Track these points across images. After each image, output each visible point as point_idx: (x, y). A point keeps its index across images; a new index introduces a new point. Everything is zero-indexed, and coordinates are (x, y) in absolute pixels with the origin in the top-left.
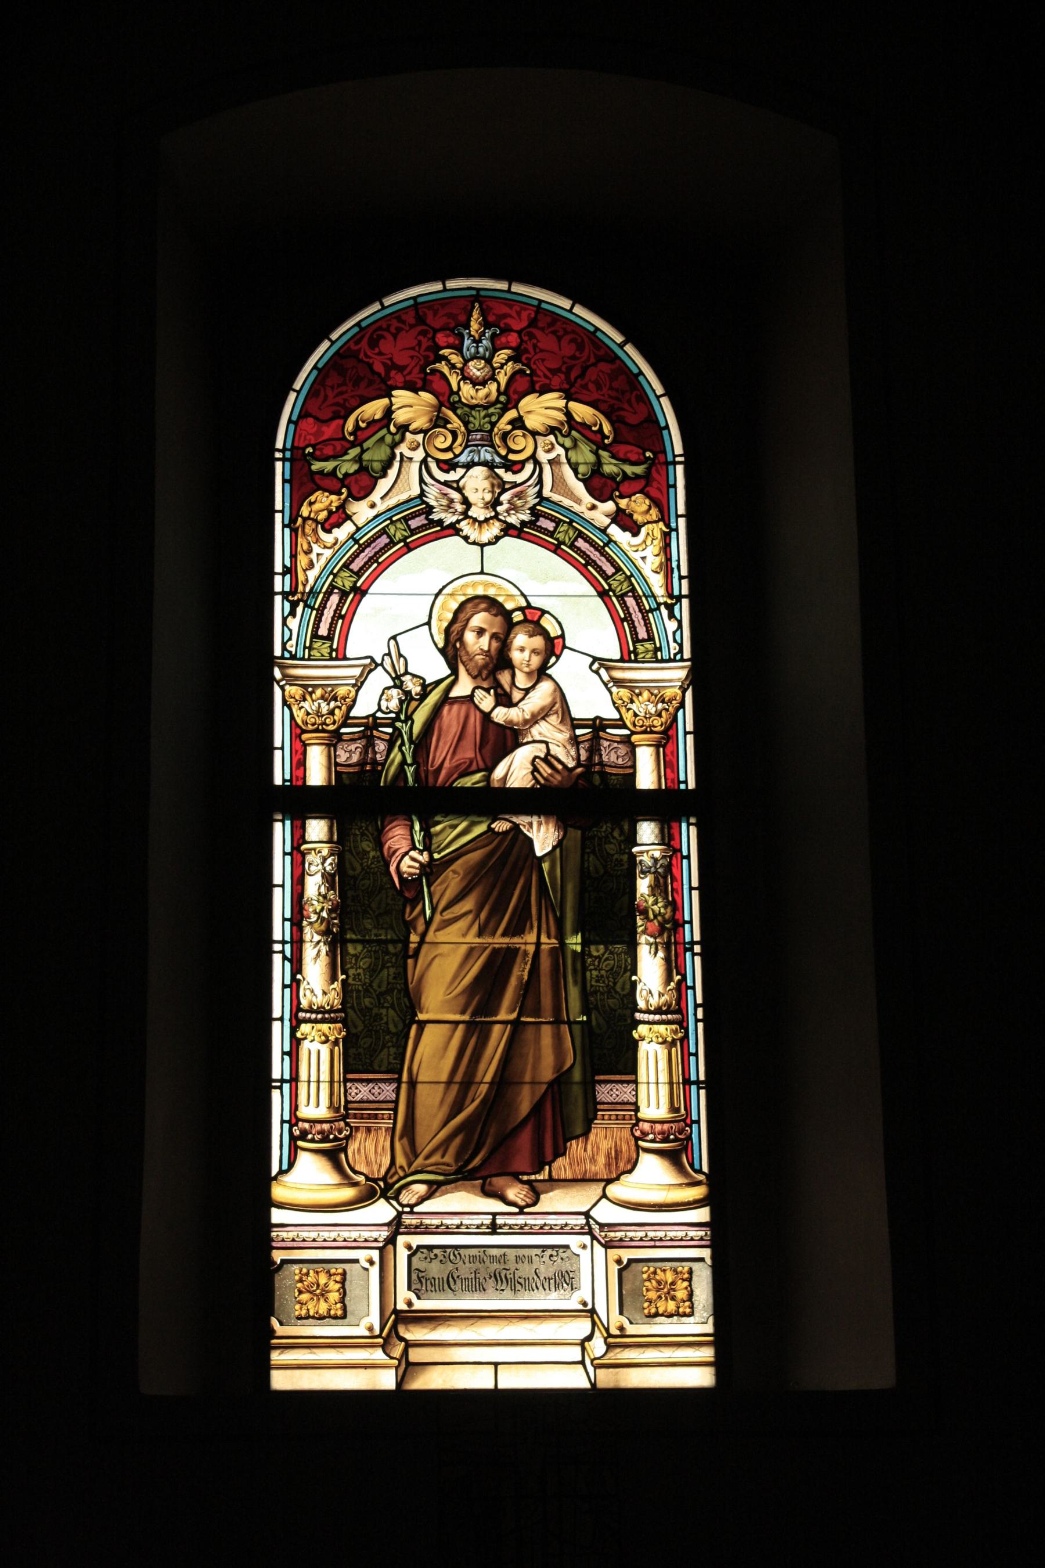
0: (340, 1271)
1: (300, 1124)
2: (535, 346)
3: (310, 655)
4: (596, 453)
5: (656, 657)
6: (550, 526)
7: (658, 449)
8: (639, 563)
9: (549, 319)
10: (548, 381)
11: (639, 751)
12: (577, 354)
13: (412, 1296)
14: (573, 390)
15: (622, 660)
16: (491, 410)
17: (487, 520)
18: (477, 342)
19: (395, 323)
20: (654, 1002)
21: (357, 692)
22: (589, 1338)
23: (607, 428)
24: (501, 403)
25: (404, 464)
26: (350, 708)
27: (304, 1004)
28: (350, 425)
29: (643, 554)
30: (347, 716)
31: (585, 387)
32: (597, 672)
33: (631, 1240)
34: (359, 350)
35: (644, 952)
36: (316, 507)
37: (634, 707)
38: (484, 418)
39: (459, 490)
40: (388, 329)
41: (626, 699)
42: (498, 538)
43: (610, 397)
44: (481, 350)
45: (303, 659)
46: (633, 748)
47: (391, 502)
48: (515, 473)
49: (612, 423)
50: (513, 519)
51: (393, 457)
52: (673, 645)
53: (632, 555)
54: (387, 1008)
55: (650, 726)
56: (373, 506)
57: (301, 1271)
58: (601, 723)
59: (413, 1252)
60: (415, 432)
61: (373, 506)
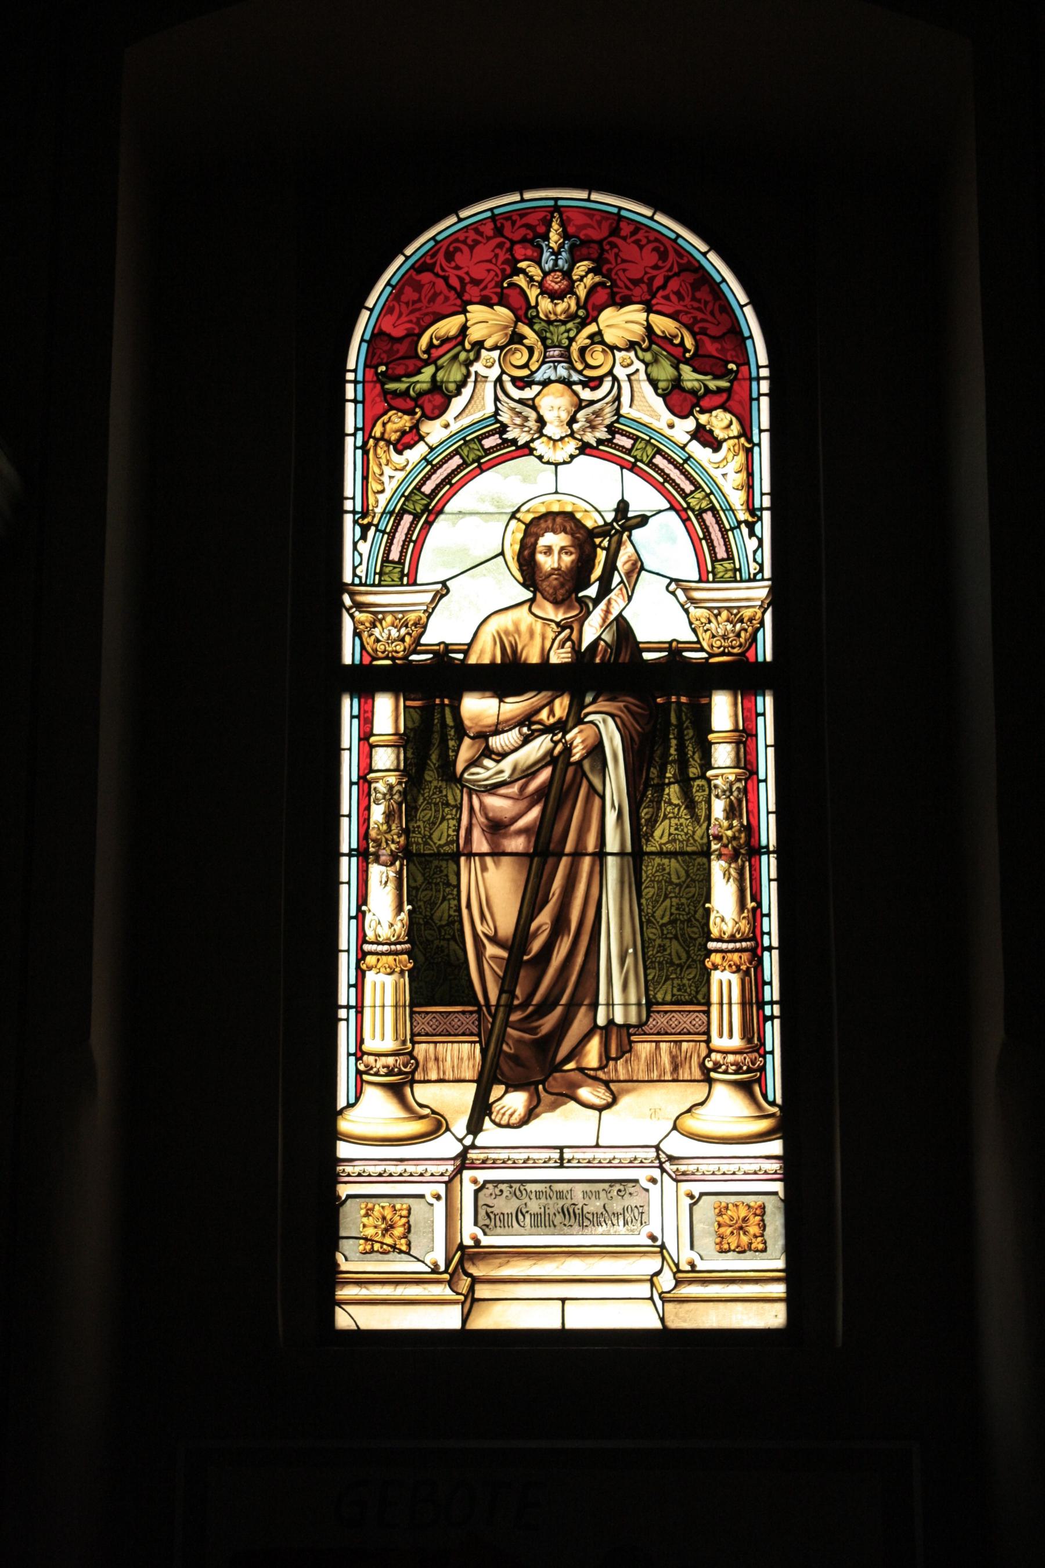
0: (405, 1206)
2: (617, 255)
3: (380, 580)
5: (735, 577)
6: (627, 443)
8: (720, 480)
9: (632, 228)
10: (629, 293)
12: (660, 263)
14: (654, 301)
16: (570, 325)
18: (556, 254)
19: (472, 235)
21: (428, 618)
23: (689, 343)
32: (673, 593)
36: (389, 426)
39: (534, 408)
40: (464, 242)
44: (560, 262)
47: (465, 421)
48: (593, 389)
49: (694, 334)
56: (447, 426)
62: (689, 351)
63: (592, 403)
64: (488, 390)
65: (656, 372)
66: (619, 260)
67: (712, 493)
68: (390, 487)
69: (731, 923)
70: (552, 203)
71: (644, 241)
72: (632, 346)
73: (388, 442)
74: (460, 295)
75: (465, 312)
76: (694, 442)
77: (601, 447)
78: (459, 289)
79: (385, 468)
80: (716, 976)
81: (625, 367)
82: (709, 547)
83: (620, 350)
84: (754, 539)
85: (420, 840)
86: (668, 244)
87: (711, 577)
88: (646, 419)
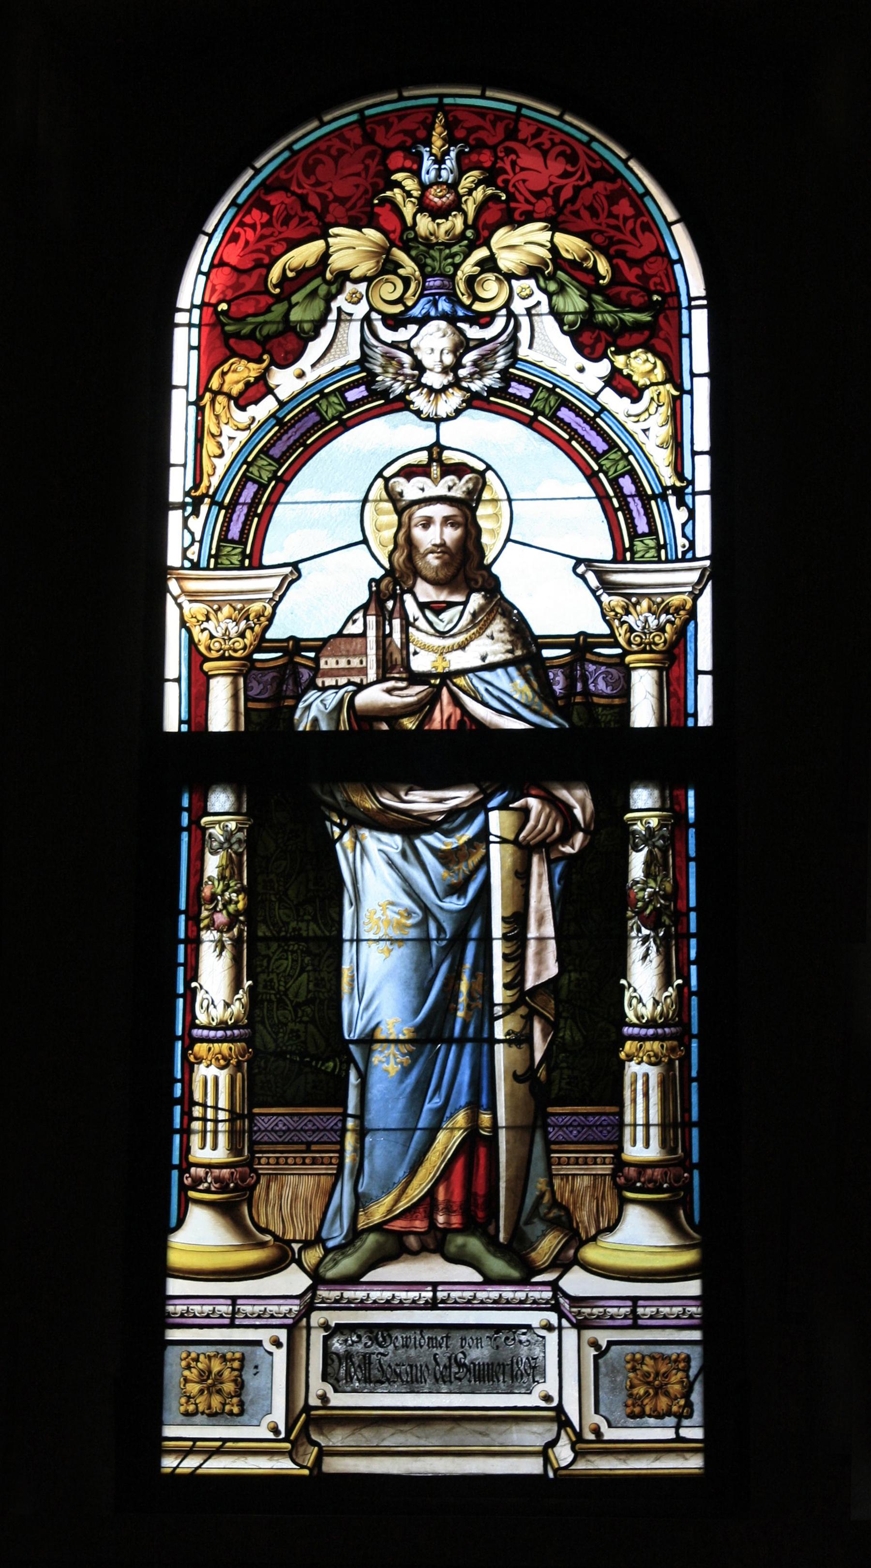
0: (238, 1355)
1: (193, 1170)
2: (514, 164)
3: (216, 563)
4: (588, 299)
5: (659, 556)
6: (525, 392)
7: (668, 290)
8: (640, 437)
9: (532, 129)
10: (530, 208)
11: (635, 676)
12: (570, 169)
13: (329, 1389)
14: (561, 218)
15: (614, 561)
16: (455, 249)
17: (444, 389)
18: (439, 161)
19: (337, 144)
20: (647, 1012)
21: (275, 608)
22: (553, 1444)
23: (603, 267)
24: (467, 238)
25: (342, 324)
26: (266, 629)
27: (202, 1018)
28: (275, 274)
29: (645, 426)
30: (262, 638)
31: (576, 214)
32: (582, 577)
33: (612, 1317)
34: (290, 180)
35: (636, 949)
36: (230, 377)
37: (630, 619)
38: (446, 258)
39: (410, 351)
40: (327, 152)
41: (619, 610)
42: (458, 412)
43: (608, 226)
44: (444, 173)
45: (208, 568)
46: (627, 671)
47: (323, 370)
48: (483, 326)
49: (610, 259)
50: (476, 386)
51: (328, 310)
52: (681, 541)
53: (630, 426)
54: (308, 922)
55: (650, 644)
56: (301, 375)
57: (189, 1354)
58: (585, 640)
59: (332, 1331)
60: (356, 281)
61: (301, 375)
62: (604, 278)
63: (482, 342)
64: (353, 333)
65: (560, 303)
66: (517, 169)
67: (631, 452)
68: (231, 450)
69: (650, 1004)
70: (435, 101)
71: (547, 145)
72: (532, 272)
73: (229, 396)
74: (320, 217)
75: (325, 236)
76: (608, 389)
77: (492, 399)
78: (319, 209)
79: (224, 428)
80: (633, 1068)
81: (524, 298)
82: (626, 519)
83: (518, 278)
84: (683, 509)
85: (273, 997)
86: (579, 149)
87: (628, 555)
88: (547, 363)
